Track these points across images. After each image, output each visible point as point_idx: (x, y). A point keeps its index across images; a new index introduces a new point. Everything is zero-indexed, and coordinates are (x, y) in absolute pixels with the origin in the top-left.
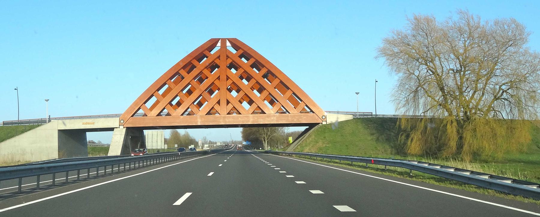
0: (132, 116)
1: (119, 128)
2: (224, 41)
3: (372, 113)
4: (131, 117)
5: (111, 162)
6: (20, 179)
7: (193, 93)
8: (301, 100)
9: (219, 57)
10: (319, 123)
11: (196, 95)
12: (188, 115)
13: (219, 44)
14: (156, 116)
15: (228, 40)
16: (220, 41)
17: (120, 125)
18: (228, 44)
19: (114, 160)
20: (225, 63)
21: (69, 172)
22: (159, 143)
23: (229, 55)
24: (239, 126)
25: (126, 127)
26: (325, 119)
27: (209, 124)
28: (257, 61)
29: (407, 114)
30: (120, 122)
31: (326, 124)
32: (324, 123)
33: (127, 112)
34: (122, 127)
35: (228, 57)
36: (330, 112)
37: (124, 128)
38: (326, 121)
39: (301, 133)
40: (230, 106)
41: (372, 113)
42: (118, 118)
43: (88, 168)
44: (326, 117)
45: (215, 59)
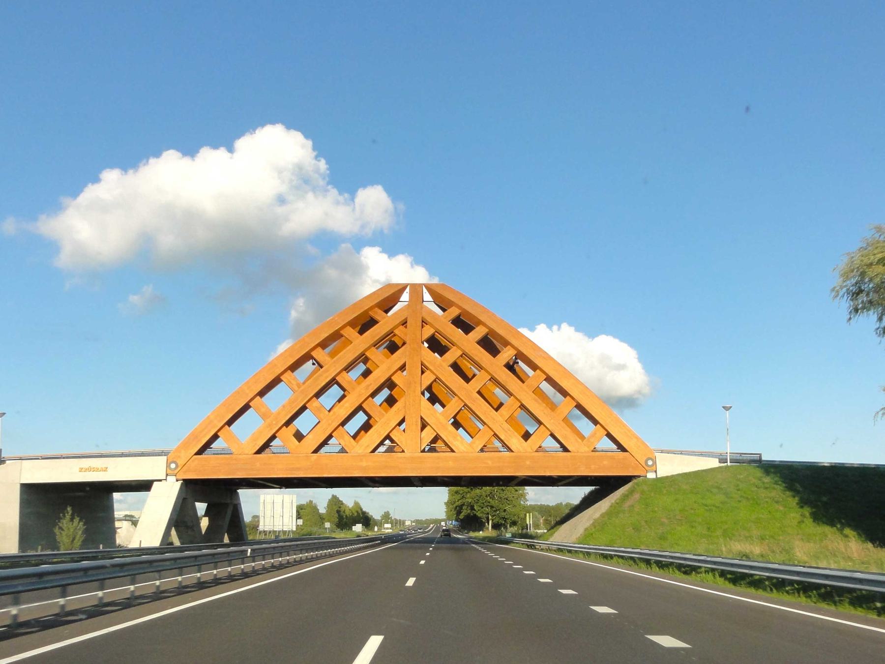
0: (200, 452)
1: (166, 480)
2: (416, 289)
3: (760, 455)
4: (196, 454)
5: (225, 555)
6: (133, 576)
7: (397, 401)
8: (484, 423)
9: (404, 323)
10: (639, 476)
11: (347, 405)
12: (386, 451)
13: (405, 297)
14: (312, 453)
15: (425, 286)
16: (408, 290)
17: (167, 475)
18: (427, 297)
19: (309, 540)
20: (419, 333)
21: (283, 553)
22: (287, 520)
23: (428, 319)
24: (463, 483)
25: (184, 480)
26: (652, 465)
27: (437, 473)
28: (492, 332)
29: (247, 529)
30: (168, 466)
31: (655, 477)
32: (651, 475)
33: (185, 445)
34: (172, 479)
35: (424, 322)
36: (662, 452)
37: (177, 481)
38: (656, 472)
39: (573, 506)
40: (428, 435)
41: (760, 455)
42: (165, 458)
43: (241, 558)
44: (655, 463)
45: (396, 327)
